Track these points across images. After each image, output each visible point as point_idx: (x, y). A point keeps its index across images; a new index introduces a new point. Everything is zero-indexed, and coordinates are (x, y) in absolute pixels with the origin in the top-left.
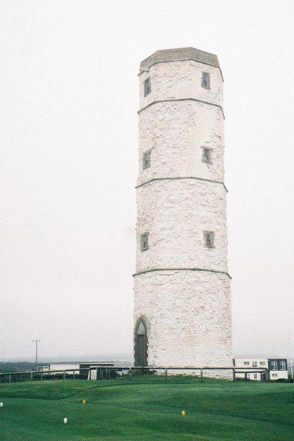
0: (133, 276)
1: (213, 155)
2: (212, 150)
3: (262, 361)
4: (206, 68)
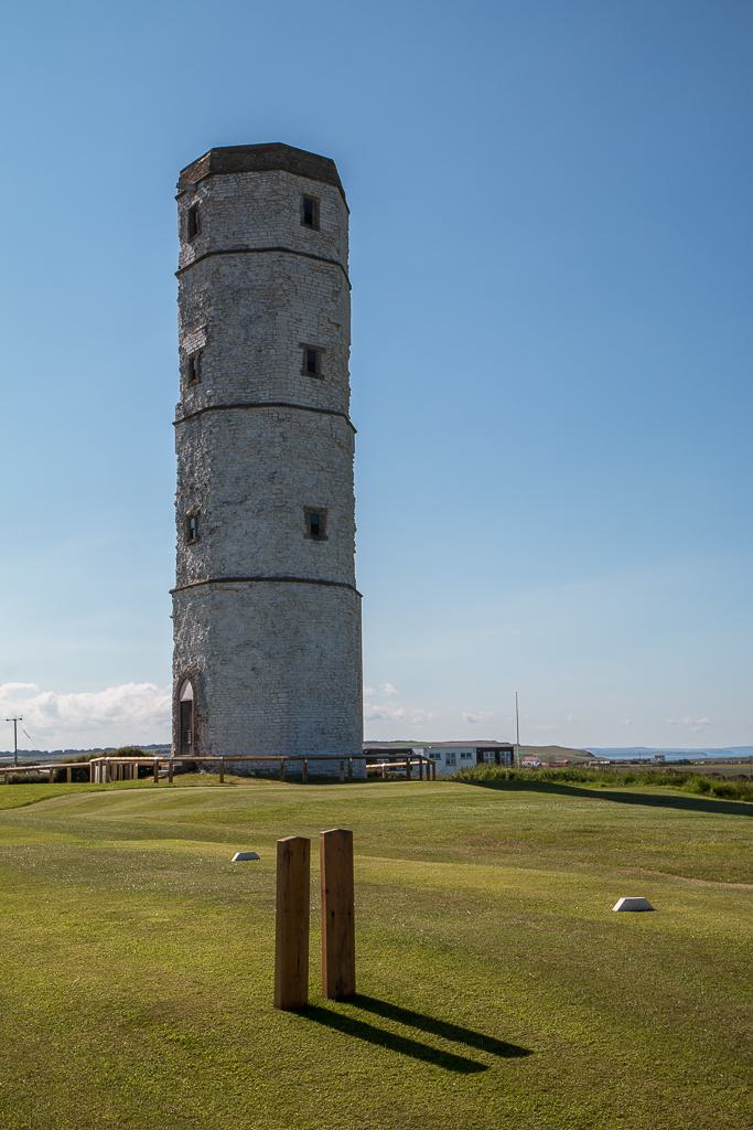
1: (324, 360)
3: (465, 751)
4: (311, 187)
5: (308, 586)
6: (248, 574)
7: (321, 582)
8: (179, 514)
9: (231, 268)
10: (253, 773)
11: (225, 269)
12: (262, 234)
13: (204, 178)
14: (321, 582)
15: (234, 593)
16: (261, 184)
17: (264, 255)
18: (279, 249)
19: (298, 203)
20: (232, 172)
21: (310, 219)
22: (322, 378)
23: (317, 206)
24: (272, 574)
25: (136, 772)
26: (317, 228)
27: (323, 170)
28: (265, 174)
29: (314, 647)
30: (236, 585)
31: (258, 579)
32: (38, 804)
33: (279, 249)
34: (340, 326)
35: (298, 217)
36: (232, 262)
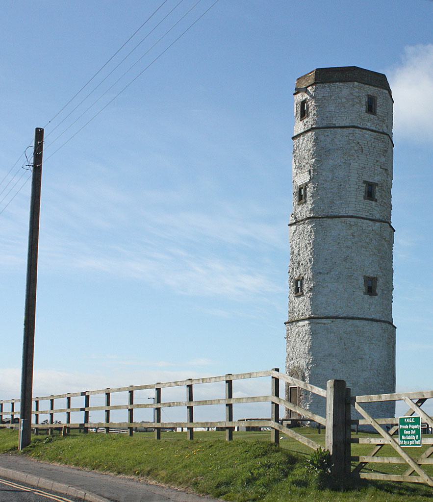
0: (285, 323)
2: (377, 184)
4: (371, 90)
5: (365, 322)
6: (331, 314)
7: (372, 320)
8: (291, 277)
11: (322, 138)
14: (372, 320)
22: (376, 295)
24: (345, 315)
29: (368, 357)
30: (324, 321)
31: (337, 318)
34: (388, 172)
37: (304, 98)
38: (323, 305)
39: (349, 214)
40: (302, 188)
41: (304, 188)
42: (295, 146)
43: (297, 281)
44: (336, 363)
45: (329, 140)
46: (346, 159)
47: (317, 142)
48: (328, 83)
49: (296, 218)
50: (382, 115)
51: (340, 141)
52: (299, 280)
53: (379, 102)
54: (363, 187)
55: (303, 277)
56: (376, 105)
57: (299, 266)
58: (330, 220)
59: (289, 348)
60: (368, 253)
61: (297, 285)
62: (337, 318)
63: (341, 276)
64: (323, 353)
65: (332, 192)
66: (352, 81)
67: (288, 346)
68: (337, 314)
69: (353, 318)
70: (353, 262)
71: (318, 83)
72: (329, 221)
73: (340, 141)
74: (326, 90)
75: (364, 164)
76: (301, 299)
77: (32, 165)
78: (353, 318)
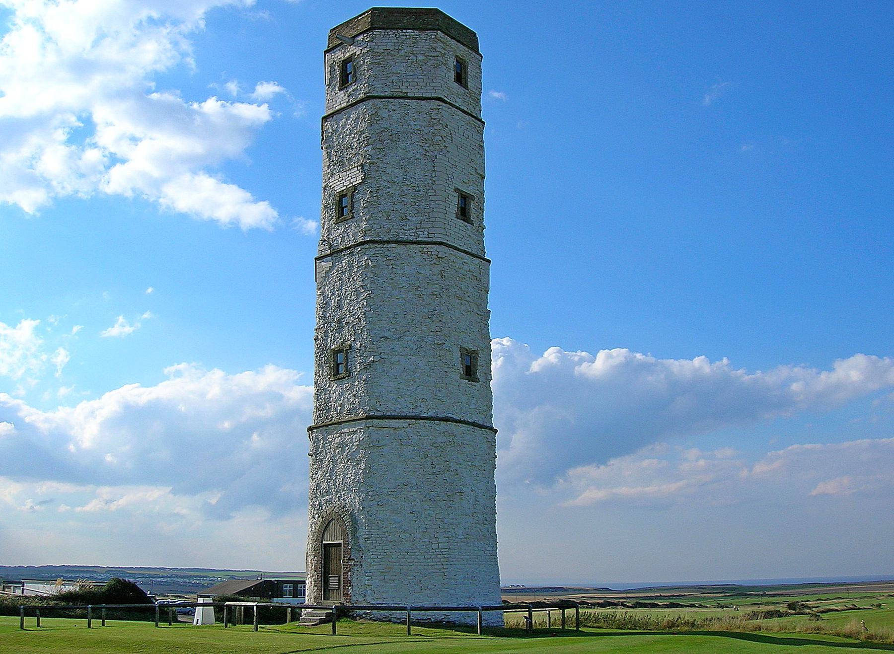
4: (462, 50)
5: (464, 427)
6: (406, 412)
8: (322, 349)
9: (391, 113)
10: (697, 605)
11: (384, 113)
12: (421, 84)
13: (367, 31)
15: (392, 431)
16: (424, 40)
17: (423, 102)
18: (438, 99)
19: (452, 62)
20: (391, 29)
21: (460, 78)
23: (466, 68)
24: (431, 414)
25: (289, 616)
26: (466, 87)
27: (468, 39)
28: (424, 35)
29: (469, 490)
30: (394, 423)
31: (417, 418)
32: (375, 645)
33: (438, 99)
35: (452, 75)
36: (391, 107)
37: (348, 55)
38: (392, 396)
39: (434, 240)
40: (345, 195)
41: (349, 194)
42: (330, 130)
43: (336, 352)
44: (418, 500)
45: (395, 117)
46: (427, 149)
47: (374, 119)
48: (394, 29)
49: (331, 246)
50: (476, 91)
51: (415, 120)
52: (340, 351)
53: (471, 70)
54: (455, 200)
55: (350, 345)
56: (466, 73)
57: (340, 328)
58: (402, 247)
59: (320, 473)
60: (463, 308)
61: (336, 360)
62: (417, 418)
63: (423, 344)
64: (393, 481)
65: (403, 201)
66: (434, 29)
67: (318, 469)
68: (417, 412)
69: (446, 420)
70: (444, 320)
71: (375, 28)
72: (400, 249)
73: (415, 120)
74: (386, 40)
75: (455, 161)
76: (346, 384)
77: (25, 419)
78: (446, 420)
